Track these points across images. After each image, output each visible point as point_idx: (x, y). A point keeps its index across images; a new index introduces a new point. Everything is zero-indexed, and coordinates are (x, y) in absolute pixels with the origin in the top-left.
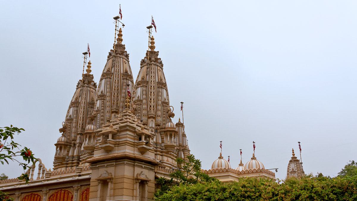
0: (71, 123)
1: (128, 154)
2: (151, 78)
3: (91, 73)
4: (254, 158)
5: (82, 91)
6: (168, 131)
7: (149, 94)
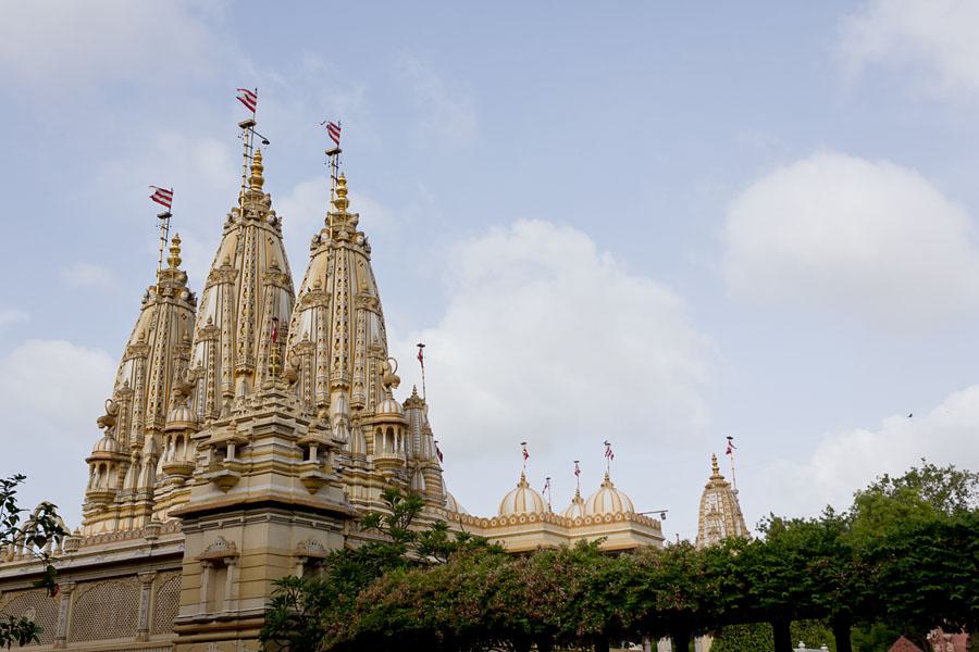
3: (181, 268)
4: (607, 484)
6: (381, 423)
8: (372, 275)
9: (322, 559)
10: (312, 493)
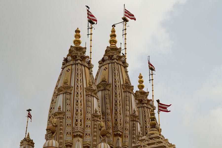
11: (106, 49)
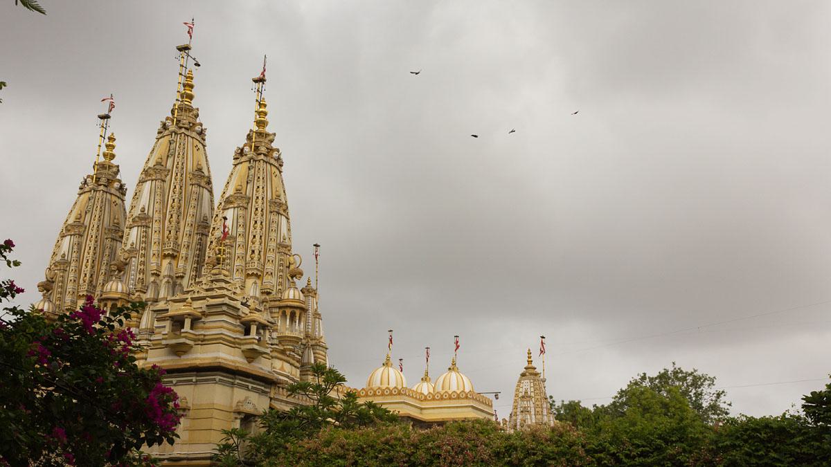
0: (66, 271)
1: (223, 361)
2: (257, 191)
3: (114, 162)
5: (92, 201)
6: (287, 307)
7: (252, 225)
8: (283, 185)
9: (255, 416)
10: (249, 363)
11: (271, 133)
